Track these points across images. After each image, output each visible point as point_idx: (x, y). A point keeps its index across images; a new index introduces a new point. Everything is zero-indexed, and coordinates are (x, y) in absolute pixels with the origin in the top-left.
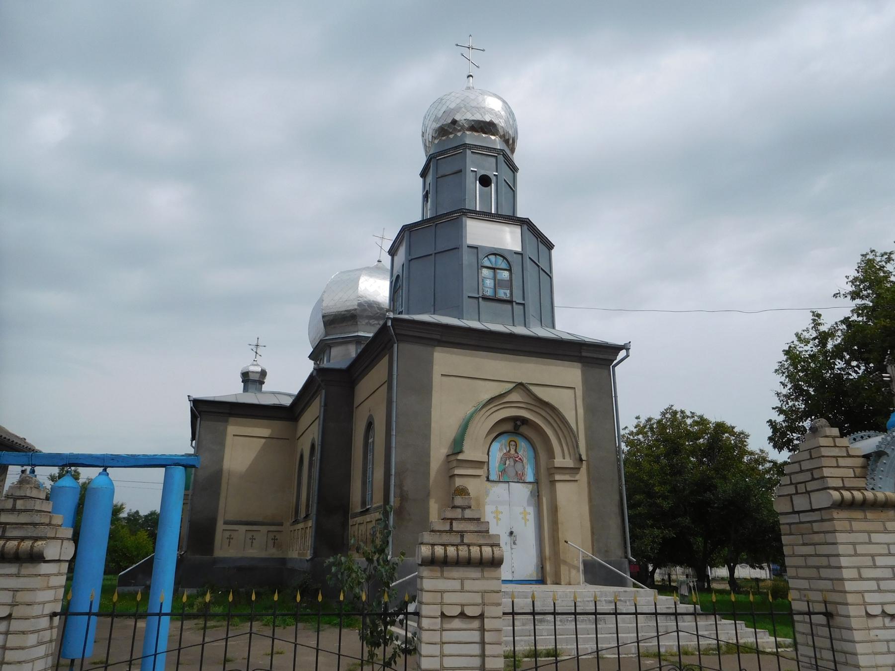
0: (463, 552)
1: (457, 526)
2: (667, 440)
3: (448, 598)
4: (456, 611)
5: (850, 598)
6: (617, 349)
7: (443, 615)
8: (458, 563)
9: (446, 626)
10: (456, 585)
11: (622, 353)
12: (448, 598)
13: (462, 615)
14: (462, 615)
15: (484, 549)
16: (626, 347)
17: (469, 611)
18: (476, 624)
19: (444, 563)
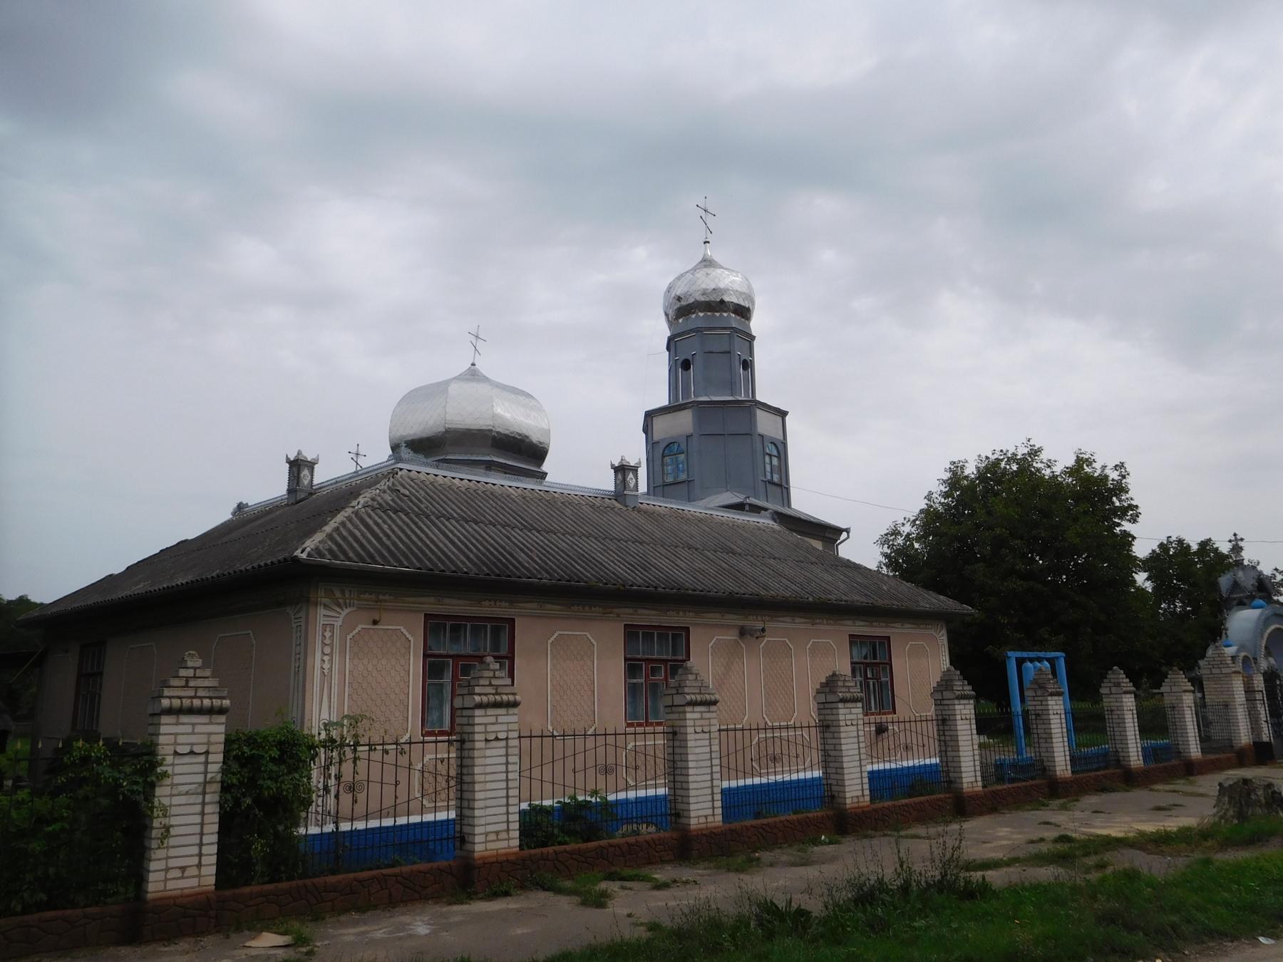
0: (197, 702)
1: (192, 683)
2: (308, 601)
3: (181, 739)
4: (186, 749)
5: (477, 729)
6: (839, 531)
7: (486, 740)
8: (191, 711)
9: (177, 761)
10: (188, 729)
11: (844, 535)
12: (181, 739)
13: (192, 753)
14: (497, 739)
15: (174, 701)
16: (848, 531)
17: (197, 749)
18: (202, 759)
19: (180, 711)
